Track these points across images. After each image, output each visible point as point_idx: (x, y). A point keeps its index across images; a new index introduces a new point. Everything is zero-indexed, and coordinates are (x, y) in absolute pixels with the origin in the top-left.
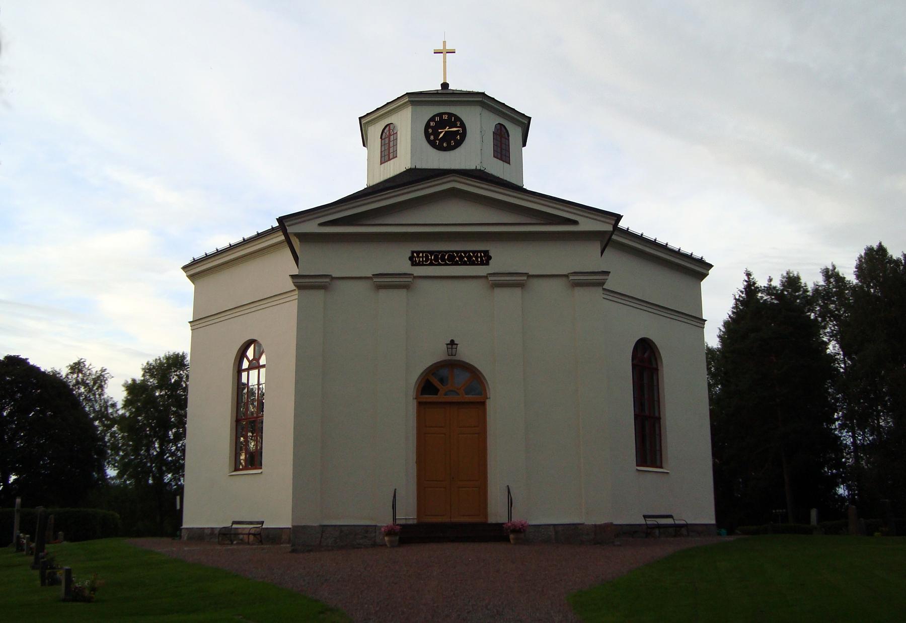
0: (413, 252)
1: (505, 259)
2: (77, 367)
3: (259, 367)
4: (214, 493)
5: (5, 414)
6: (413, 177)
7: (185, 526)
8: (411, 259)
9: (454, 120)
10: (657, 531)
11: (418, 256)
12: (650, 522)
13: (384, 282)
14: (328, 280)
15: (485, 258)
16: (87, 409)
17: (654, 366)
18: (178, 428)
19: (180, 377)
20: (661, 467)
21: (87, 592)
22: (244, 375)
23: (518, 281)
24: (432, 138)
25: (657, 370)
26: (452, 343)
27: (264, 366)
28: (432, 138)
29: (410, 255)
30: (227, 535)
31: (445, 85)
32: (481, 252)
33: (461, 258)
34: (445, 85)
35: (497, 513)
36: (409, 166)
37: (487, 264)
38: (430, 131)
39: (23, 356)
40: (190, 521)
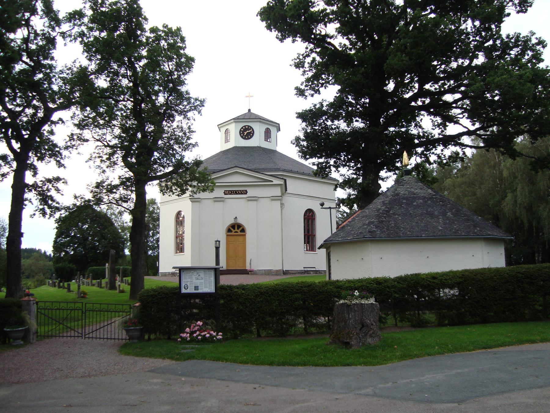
1: (251, 192)
6: (235, 149)
7: (160, 271)
9: (250, 128)
10: (312, 272)
12: (306, 269)
13: (217, 200)
15: (246, 192)
18: (154, 231)
19: (154, 208)
23: (255, 199)
31: (249, 110)
34: (249, 110)
35: (248, 268)
40: (161, 270)
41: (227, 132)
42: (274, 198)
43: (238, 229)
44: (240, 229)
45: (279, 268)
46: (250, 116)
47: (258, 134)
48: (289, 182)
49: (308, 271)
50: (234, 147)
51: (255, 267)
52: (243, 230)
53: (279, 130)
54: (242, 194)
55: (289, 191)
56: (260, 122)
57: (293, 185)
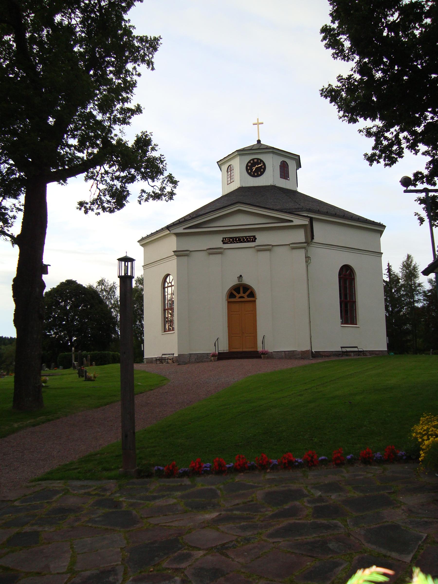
0: (223, 238)
1: (262, 238)
2: (101, 283)
3: (172, 286)
4: (157, 342)
5: (68, 308)
6: (241, 189)
8: (222, 241)
9: (260, 161)
10: (352, 354)
11: (225, 240)
12: (344, 350)
13: (212, 252)
14: (188, 252)
15: (254, 239)
16: (108, 303)
17: (353, 277)
20: (356, 324)
21: (92, 378)
22: (166, 289)
24: (249, 171)
25: (354, 279)
26: (241, 276)
27: (173, 286)
28: (249, 171)
29: (222, 239)
30: (161, 360)
31: (259, 141)
32: (252, 236)
33: (243, 239)
34: (259, 141)
36: (239, 186)
37: (255, 241)
38: (249, 168)
39: (74, 280)
41: (230, 169)
42: (294, 247)
43: (244, 293)
44: (247, 293)
45: (305, 347)
46: (260, 147)
47: (272, 168)
48: (316, 225)
49: (347, 352)
50: (240, 188)
51: (270, 348)
52: (252, 294)
53: (299, 166)
54: (249, 242)
55: (316, 240)
56: (273, 153)
57: (322, 232)
